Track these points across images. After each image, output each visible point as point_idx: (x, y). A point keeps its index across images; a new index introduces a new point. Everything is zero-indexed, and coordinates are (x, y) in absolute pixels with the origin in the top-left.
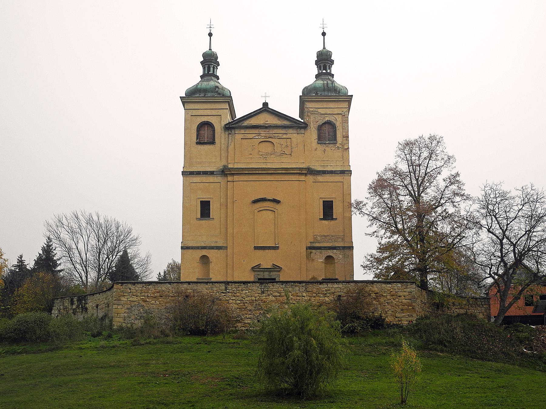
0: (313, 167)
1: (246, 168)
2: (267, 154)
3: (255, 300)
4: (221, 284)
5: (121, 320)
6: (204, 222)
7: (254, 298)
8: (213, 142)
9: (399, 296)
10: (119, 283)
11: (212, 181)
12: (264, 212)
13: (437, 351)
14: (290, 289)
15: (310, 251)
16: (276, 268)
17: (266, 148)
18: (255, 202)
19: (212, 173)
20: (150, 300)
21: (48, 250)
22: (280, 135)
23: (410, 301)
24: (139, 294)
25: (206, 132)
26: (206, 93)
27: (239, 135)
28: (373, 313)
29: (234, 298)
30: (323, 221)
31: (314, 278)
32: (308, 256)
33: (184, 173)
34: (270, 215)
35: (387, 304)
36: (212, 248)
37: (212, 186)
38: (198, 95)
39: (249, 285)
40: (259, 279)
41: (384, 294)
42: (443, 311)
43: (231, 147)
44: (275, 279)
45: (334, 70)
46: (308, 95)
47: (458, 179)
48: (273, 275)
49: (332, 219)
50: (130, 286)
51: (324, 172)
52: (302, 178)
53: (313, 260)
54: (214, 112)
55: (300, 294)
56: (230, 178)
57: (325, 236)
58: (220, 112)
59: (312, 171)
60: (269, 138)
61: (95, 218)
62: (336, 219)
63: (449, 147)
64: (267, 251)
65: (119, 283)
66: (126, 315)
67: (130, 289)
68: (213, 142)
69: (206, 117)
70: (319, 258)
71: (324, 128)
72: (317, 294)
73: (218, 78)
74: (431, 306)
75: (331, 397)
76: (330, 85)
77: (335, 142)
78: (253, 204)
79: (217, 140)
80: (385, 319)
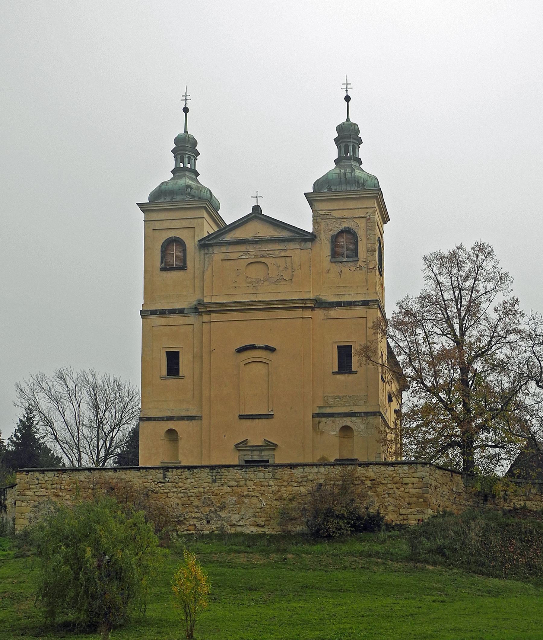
0: (324, 298)
1: (226, 303)
2: (258, 281)
3: (204, 493)
4: (157, 471)
5: (26, 522)
6: (172, 382)
7: (202, 490)
8: (182, 267)
9: (406, 484)
10: (24, 471)
11: (181, 322)
12: (254, 365)
13: (428, 563)
14: (252, 476)
15: (317, 419)
16: (271, 446)
17: (256, 272)
18: (240, 350)
19: (181, 311)
20: (64, 494)
21: (26, 428)
22: (277, 252)
23: (420, 491)
24: (49, 486)
25: (174, 253)
26: (180, 197)
27: (218, 254)
28: (367, 508)
29: (175, 490)
30: (338, 376)
31: (323, 458)
32: (316, 427)
33: (142, 313)
34: (260, 369)
35: (387, 496)
36: (182, 418)
37: (182, 329)
38: (162, 200)
39: (195, 470)
40: (246, 462)
41: (383, 482)
42: (495, 504)
43: (208, 274)
44: (268, 461)
45: (362, 153)
46: (320, 194)
47: (516, 307)
48: (266, 455)
49: (351, 372)
50: (37, 474)
51: (339, 304)
52: (308, 313)
53: (322, 433)
54: (185, 224)
55: (266, 484)
56: (206, 318)
57: (340, 397)
58: (194, 223)
59: (322, 303)
60: (261, 257)
61: (91, 379)
62: (356, 372)
63: (504, 260)
64: (257, 421)
65: (24, 471)
66: (32, 515)
67: (38, 479)
68: (182, 267)
69: (173, 231)
70: (331, 429)
71: (340, 239)
72: (290, 482)
73: (197, 174)
74: (471, 498)
75: (143, 622)
76: (348, 175)
77: (356, 259)
78: (238, 354)
79: (189, 264)
80: (384, 517)
